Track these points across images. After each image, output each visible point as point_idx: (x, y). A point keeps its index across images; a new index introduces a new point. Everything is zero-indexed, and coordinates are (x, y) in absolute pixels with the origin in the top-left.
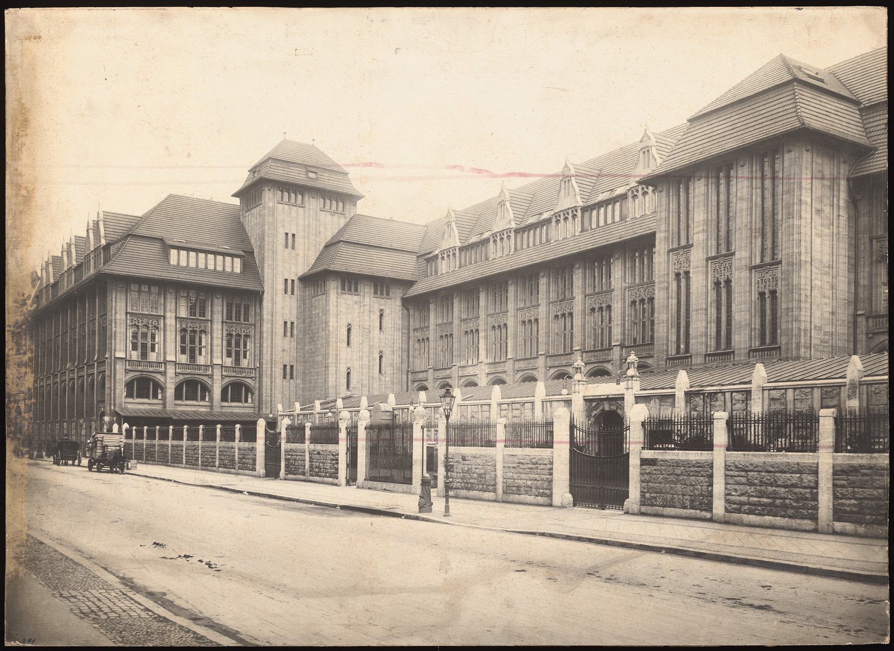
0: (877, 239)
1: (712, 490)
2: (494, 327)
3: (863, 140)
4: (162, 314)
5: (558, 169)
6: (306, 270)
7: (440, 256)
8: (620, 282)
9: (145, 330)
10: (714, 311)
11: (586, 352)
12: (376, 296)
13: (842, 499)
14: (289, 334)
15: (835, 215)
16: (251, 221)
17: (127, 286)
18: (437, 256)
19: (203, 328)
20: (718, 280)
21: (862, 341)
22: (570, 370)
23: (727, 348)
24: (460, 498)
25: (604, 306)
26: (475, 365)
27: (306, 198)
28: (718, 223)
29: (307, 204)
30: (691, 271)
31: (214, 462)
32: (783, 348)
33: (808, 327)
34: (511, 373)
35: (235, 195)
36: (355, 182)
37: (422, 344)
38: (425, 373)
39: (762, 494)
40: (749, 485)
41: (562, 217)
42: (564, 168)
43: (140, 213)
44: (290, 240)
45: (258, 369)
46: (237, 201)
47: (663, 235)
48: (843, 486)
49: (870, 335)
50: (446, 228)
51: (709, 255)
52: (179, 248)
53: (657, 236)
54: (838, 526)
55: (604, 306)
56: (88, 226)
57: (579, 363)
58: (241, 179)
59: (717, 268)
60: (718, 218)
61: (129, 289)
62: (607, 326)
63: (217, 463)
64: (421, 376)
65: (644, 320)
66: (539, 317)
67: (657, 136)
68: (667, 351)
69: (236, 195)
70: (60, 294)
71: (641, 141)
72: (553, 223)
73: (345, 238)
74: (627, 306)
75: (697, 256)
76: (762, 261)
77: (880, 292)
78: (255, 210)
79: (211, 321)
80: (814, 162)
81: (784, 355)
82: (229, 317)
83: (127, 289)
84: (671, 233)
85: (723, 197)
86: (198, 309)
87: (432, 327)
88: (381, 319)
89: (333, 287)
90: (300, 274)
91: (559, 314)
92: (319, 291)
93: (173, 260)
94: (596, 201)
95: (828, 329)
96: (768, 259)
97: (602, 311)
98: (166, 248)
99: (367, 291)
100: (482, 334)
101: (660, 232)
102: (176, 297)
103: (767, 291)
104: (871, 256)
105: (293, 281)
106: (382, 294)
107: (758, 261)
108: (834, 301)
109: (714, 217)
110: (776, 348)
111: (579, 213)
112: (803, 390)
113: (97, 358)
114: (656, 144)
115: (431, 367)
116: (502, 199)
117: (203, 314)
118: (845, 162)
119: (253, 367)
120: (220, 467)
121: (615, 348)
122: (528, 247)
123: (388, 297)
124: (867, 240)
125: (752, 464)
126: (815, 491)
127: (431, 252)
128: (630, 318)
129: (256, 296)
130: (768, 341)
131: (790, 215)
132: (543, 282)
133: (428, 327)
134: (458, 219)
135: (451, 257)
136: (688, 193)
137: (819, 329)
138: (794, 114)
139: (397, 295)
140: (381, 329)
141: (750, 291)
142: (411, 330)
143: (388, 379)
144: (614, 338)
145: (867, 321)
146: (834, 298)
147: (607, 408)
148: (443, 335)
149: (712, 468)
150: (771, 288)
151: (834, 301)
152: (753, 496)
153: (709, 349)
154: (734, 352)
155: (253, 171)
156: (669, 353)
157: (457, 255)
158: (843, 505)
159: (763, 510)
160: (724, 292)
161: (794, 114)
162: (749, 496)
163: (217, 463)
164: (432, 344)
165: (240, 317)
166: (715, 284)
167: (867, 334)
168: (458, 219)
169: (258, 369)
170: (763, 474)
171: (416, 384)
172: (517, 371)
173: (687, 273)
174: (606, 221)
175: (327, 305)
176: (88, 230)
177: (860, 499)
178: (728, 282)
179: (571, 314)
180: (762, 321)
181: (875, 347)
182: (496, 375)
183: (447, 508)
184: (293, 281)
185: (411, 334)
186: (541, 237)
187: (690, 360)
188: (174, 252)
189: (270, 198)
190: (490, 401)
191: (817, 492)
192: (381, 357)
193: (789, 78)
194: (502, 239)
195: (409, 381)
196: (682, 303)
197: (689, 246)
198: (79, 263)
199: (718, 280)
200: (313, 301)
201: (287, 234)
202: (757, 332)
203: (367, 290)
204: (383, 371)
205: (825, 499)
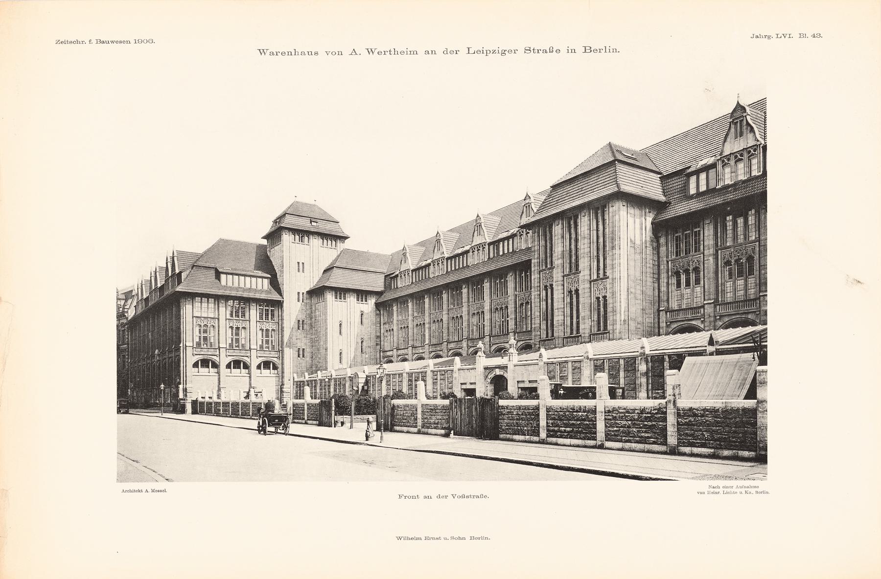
0: (671, 261)
1: (539, 423)
2: (434, 321)
3: (663, 198)
4: (217, 317)
5: (431, 234)
6: (312, 286)
7: (399, 275)
8: (513, 291)
9: (205, 328)
10: (569, 309)
11: (431, 345)
12: (358, 302)
13: (609, 427)
14: (301, 328)
15: (643, 247)
16: (274, 255)
17: (193, 299)
18: (397, 276)
19: (244, 326)
20: (570, 289)
21: (663, 327)
22: (507, 345)
23: (577, 333)
24: (625, 450)
25: (503, 306)
26: (460, 341)
27: (311, 240)
28: (570, 252)
29: (311, 244)
30: (554, 284)
31: (249, 413)
32: (611, 332)
33: (626, 318)
34: (446, 351)
35: (264, 238)
36: (345, 228)
37: (389, 333)
38: (406, 350)
39: (566, 426)
40: (560, 420)
41: (476, 249)
42: (477, 217)
43: (201, 250)
44: (301, 267)
45: (281, 351)
46: (265, 242)
47: (536, 261)
48: (610, 420)
49: (668, 323)
50: (403, 257)
51: (565, 273)
52: (227, 274)
53: (533, 261)
54: (232, 416)
55: (503, 306)
56: (167, 260)
57: (512, 341)
58: (267, 228)
59: (576, 280)
60: (570, 249)
61: (194, 301)
62: (461, 327)
63: (251, 414)
64: (389, 353)
65: (508, 319)
66: (463, 315)
67: (484, 216)
68: (540, 335)
69: (264, 238)
70: (166, 293)
71: (525, 200)
72: (399, 277)
73: (337, 264)
74: (518, 306)
75: (557, 275)
76: (598, 277)
77: (674, 295)
78: (277, 247)
79: (249, 321)
80: (628, 213)
81: (611, 336)
82: (261, 318)
83: (193, 301)
84: (541, 259)
85: (573, 236)
86: (238, 313)
87: (395, 322)
88: (362, 317)
89: (330, 297)
90: (308, 289)
91: (476, 312)
92: (320, 299)
93: (223, 282)
94: (498, 239)
95: (640, 319)
96: (601, 276)
97: (503, 310)
98: (218, 274)
99: (352, 299)
100: (427, 326)
101: (534, 259)
102: (226, 306)
103: (601, 296)
104: (668, 273)
105: (303, 293)
106: (362, 301)
107: (595, 277)
108: (644, 302)
109: (568, 248)
110: (607, 333)
111: (487, 247)
112: (613, 360)
113: (168, 349)
114: (534, 201)
115: (465, 338)
116: (404, 251)
117: (244, 315)
118: (650, 212)
119: (277, 350)
120: (253, 416)
121: (511, 334)
122: (426, 278)
123: (366, 303)
124: (665, 262)
125: (561, 408)
126: (595, 423)
127: (689, 167)
128: (520, 314)
129: (279, 304)
130: (602, 329)
131: (613, 248)
132: (486, 285)
133: (392, 322)
134: (535, 201)
135: (406, 276)
136: (603, 216)
137: (634, 320)
138: (614, 183)
139: (372, 301)
140: (362, 323)
141: (591, 296)
142: (382, 324)
143: (367, 356)
144: (510, 328)
145: (515, 335)
146: (644, 299)
147: (498, 374)
148: (403, 327)
149: (539, 410)
150: (603, 295)
151: (644, 302)
152: (562, 427)
153: (566, 334)
154: (609, 332)
155: (275, 222)
156: (542, 337)
157: (410, 274)
158: (610, 431)
159: (567, 435)
160: (574, 297)
161: (614, 183)
162: (560, 427)
163: (251, 414)
164: (395, 333)
165: (268, 318)
166: (569, 292)
167: (666, 323)
168: (486, 221)
169: (281, 351)
170: (567, 413)
171: (386, 359)
172: (671, 322)
173: (551, 285)
174: (394, 287)
175: (326, 307)
176: (167, 263)
177: (619, 427)
178: (577, 291)
179: (483, 312)
180: (598, 315)
181: (671, 331)
182: (455, 350)
183: (381, 437)
184: (303, 293)
185: (382, 327)
186: (459, 264)
187: (608, 334)
188: (223, 277)
189: (287, 237)
190: (452, 368)
191: (596, 424)
192: (362, 342)
193: (612, 159)
194: (438, 264)
195: (381, 357)
196: (549, 305)
197: (552, 268)
198: (162, 284)
199: (570, 289)
200: (317, 306)
201: (298, 263)
202: (595, 322)
203: (352, 298)
204: (364, 351)
205: (601, 426)
